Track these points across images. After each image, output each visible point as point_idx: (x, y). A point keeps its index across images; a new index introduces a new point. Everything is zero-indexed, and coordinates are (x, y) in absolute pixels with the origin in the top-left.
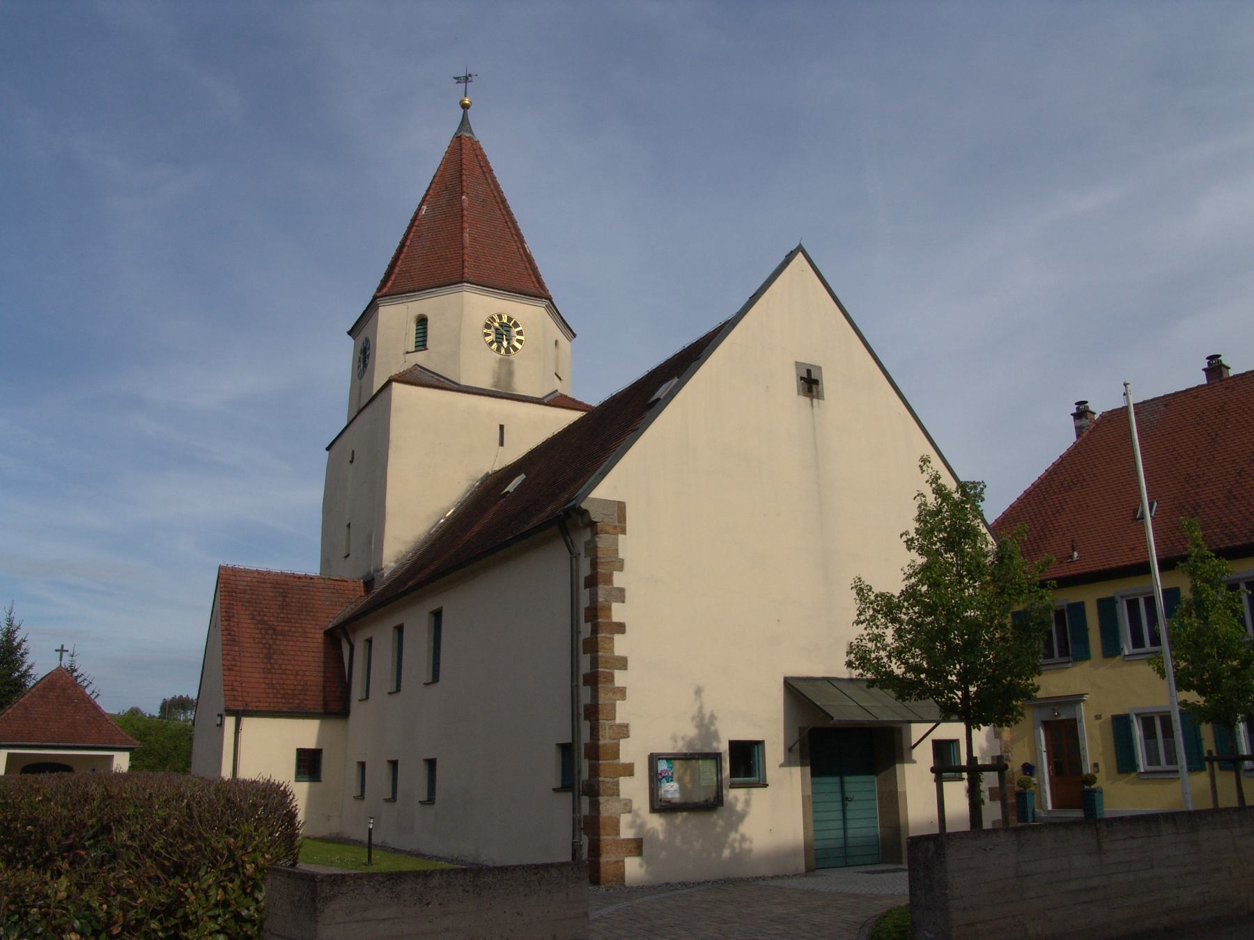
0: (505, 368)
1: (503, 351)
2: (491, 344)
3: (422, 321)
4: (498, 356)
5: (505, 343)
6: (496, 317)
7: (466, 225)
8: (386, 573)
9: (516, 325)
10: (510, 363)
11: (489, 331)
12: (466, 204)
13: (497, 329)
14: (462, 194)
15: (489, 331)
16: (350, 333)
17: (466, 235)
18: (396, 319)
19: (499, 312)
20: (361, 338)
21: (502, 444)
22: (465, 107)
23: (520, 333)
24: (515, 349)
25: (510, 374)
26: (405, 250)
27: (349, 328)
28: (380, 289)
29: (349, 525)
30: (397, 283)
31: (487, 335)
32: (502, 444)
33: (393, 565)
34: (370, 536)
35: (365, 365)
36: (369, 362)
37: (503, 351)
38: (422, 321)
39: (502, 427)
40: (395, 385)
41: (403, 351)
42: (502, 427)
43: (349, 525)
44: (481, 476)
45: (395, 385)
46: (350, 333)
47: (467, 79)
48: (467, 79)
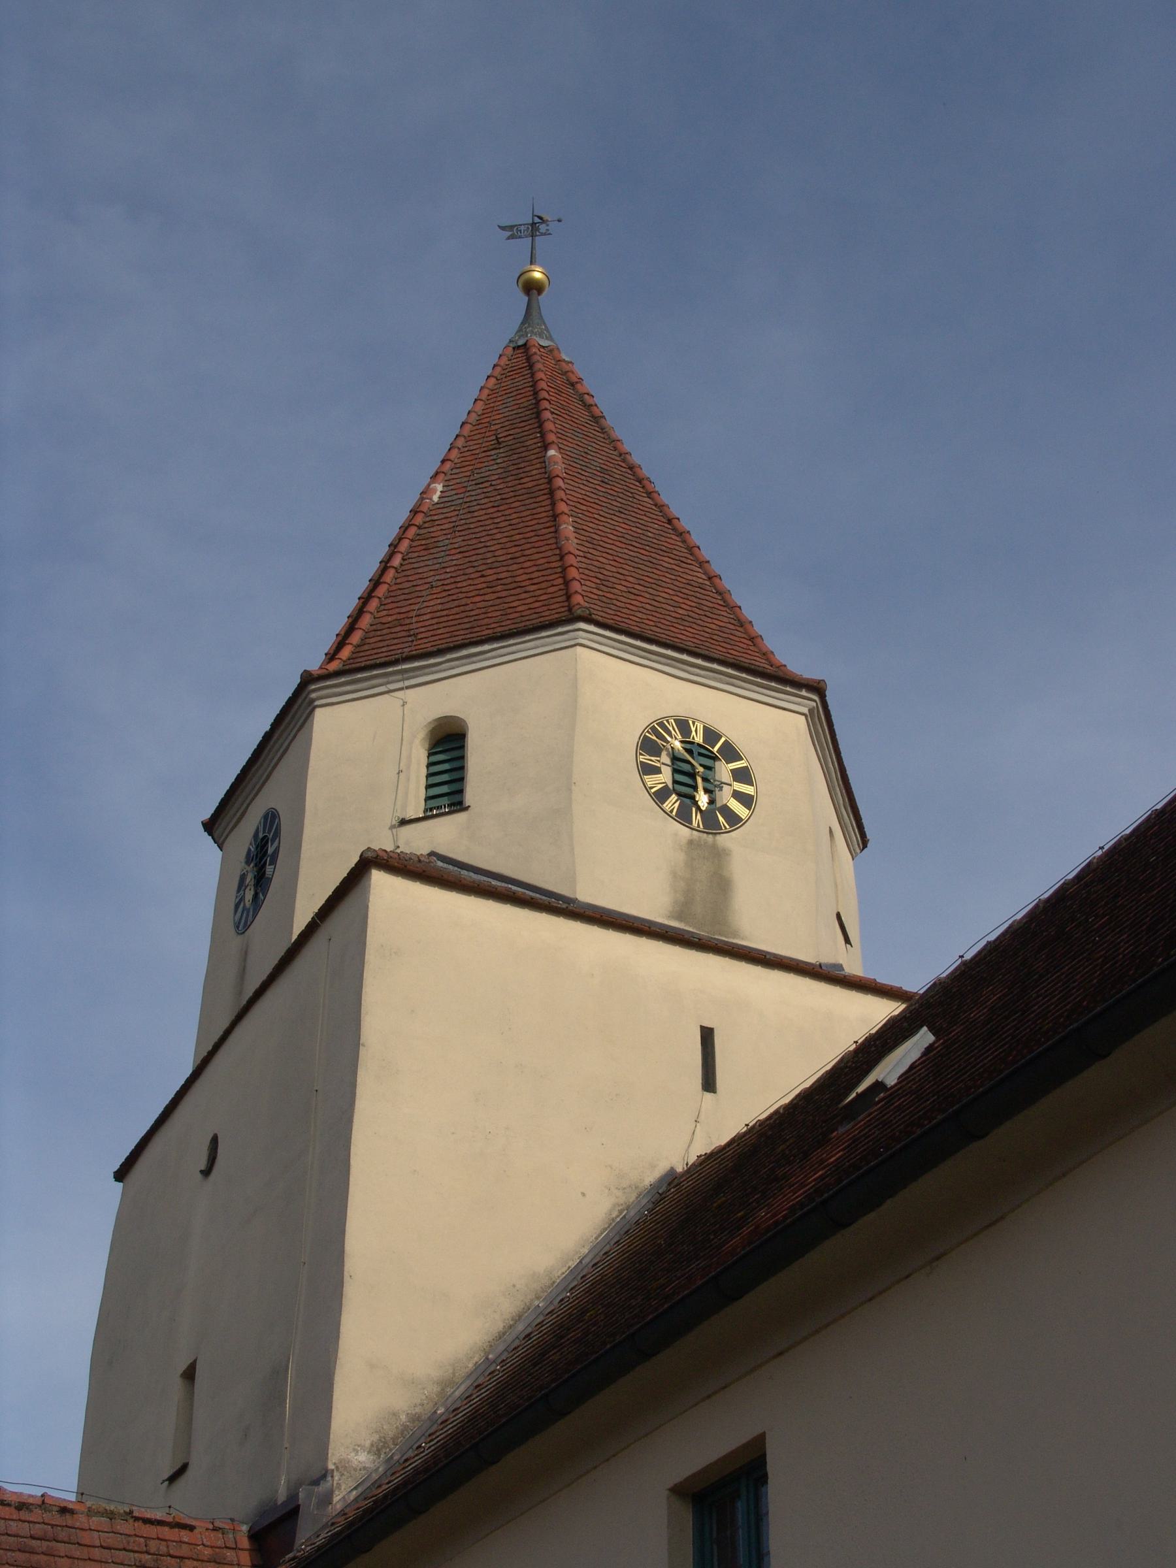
0: (710, 880)
1: (696, 819)
2: (661, 796)
3: (448, 743)
4: (684, 831)
5: (703, 799)
6: (672, 726)
7: (562, 507)
8: (343, 1493)
9: (731, 753)
10: (719, 856)
11: (652, 760)
12: (559, 468)
13: (675, 758)
14: (546, 448)
15: (652, 760)
16: (210, 826)
17: (567, 528)
18: (365, 747)
19: (682, 712)
20: (243, 836)
21: (709, 1084)
22: (532, 288)
23: (743, 775)
24: (734, 820)
25: (722, 886)
26: (390, 576)
27: (207, 815)
28: (331, 656)
29: (189, 1374)
30: (380, 642)
31: (647, 770)
32: (709, 1084)
33: (363, 1458)
34: (278, 1373)
35: (262, 882)
36: (278, 875)
37: (696, 819)
38: (448, 743)
39: (707, 1035)
40: (378, 878)
41: (390, 819)
42: (707, 1035)
43: (189, 1374)
44: (651, 1177)
45: (378, 878)
46: (210, 826)
47: (535, 227)
48: (535, 227)
